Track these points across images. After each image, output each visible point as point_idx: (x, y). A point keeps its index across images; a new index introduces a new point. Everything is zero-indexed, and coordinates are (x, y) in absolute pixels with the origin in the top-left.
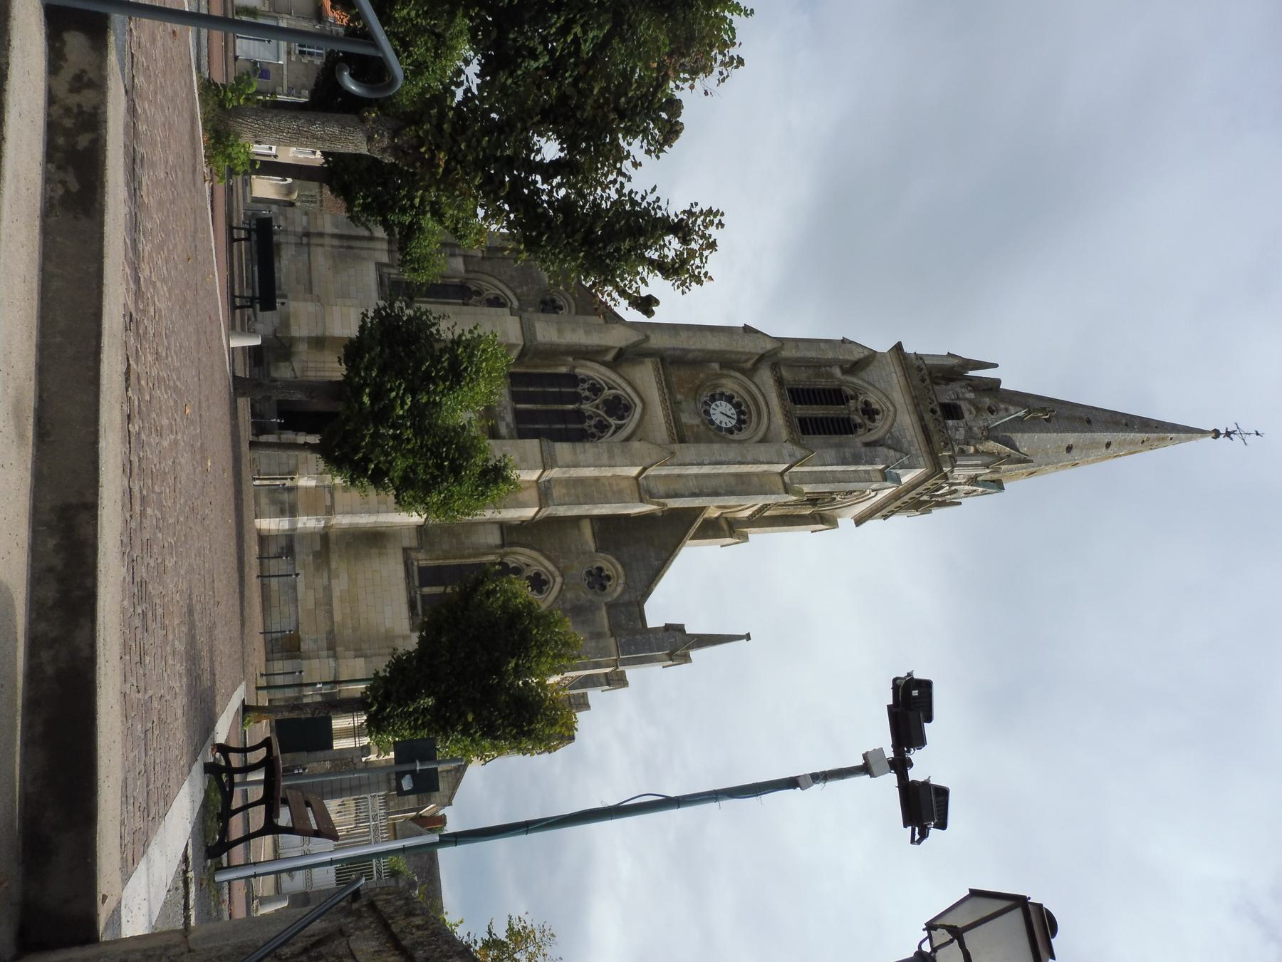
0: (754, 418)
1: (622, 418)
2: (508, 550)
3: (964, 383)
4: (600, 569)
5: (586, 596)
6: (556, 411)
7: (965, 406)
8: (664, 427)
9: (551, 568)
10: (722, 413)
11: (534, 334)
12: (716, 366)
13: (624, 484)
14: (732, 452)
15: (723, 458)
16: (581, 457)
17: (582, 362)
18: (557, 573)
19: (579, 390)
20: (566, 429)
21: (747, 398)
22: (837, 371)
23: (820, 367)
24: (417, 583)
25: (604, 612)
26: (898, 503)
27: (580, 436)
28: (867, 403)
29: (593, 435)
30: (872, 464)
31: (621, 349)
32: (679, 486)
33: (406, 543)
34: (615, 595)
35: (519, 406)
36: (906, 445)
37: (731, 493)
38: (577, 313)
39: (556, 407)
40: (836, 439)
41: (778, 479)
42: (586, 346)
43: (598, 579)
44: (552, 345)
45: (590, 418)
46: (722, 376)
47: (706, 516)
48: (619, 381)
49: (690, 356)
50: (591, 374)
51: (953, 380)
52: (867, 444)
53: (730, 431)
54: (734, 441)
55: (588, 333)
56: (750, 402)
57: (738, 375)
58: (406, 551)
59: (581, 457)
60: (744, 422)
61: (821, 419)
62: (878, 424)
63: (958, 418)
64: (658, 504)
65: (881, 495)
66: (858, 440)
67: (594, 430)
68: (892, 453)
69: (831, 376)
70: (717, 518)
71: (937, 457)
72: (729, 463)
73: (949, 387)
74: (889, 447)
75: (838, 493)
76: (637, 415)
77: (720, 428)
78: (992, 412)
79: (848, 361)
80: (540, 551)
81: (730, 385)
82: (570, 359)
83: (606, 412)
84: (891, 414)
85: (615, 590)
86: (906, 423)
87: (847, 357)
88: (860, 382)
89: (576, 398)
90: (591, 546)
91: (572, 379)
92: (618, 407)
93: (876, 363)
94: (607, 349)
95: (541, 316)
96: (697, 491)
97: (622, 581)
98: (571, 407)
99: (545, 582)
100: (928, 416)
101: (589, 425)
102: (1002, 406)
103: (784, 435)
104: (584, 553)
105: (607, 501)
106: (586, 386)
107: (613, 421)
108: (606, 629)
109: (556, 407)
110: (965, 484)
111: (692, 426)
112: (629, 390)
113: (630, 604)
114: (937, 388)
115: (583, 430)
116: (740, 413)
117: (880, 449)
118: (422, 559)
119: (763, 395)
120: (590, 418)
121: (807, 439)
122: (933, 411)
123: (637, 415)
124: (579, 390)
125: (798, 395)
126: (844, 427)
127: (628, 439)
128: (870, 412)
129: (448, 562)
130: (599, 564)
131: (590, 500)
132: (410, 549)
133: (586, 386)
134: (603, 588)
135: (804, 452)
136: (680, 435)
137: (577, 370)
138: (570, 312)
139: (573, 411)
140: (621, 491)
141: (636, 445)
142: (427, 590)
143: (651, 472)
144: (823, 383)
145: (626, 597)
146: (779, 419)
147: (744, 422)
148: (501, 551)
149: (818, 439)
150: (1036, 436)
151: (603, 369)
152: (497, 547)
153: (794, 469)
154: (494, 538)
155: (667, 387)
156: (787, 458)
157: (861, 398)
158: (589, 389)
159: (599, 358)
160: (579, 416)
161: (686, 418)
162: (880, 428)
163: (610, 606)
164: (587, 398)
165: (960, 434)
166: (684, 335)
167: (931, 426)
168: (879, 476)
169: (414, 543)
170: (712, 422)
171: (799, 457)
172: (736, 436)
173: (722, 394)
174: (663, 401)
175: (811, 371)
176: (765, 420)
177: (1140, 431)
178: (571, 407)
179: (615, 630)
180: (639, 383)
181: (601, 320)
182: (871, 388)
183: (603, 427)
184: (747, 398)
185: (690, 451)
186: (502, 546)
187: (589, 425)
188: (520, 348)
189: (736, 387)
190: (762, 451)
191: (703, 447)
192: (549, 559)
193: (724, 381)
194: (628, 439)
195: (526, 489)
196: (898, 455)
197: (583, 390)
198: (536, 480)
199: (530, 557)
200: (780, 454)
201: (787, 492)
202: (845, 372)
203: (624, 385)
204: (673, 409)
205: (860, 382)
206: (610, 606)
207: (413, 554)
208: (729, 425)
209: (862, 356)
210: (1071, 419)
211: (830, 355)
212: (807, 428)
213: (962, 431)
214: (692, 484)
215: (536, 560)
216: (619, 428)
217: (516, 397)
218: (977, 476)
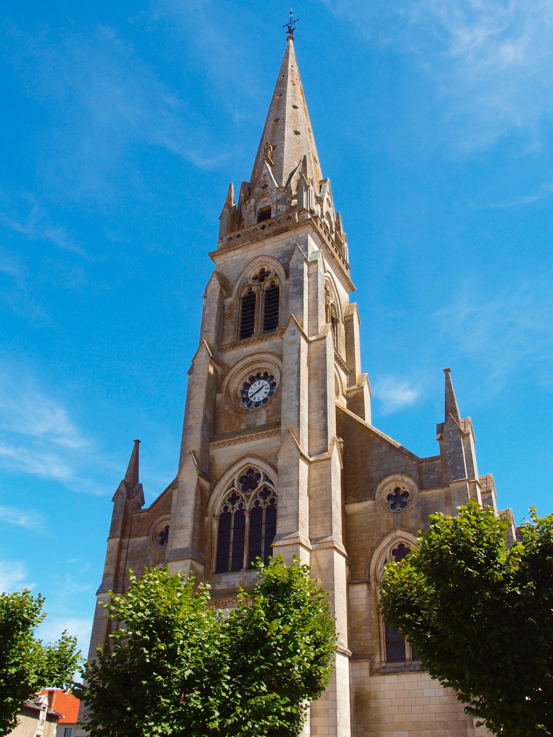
0: (263, 365)
1: (259, 476)
2: (372, 578)
3: (243, 207)
4: (390, 497)
5: (412, 510)
6: (250, 532)
7: (260, 206)
8: (267, 439)
9: (388, 540)
10: (259, 391)
11: (183, 550)
12: (219, 396)
13: (314, 473)
14: (289, 382)
15: (295, 389)
16: (290, 510)
17: (209, 509)
18: (393, 535)
19: (264, 507)
20: (234, 529)
21: (245, 371)
22: (229, 301)
23: (224, 314)
24: (402, 664)
25: (424, 493)
26: (336, 256)
27: (272, 511)
28: (255, 278)
29: (273, 500)
30: (302, 271)
31: (199, 475)
32: (317, 427)
33: (366, 673)
34: (412, 483)
35: (244, 566)
36: (289, 247)
37: (324, 383)
38: (170, 513)
39: (247, 533)
40: (282, 300)
41: (313, 345)
42: (196, 505)
43: (398, 499)
44: (193, 535)
45: (257, 502)
46: (228, 391)
47: (345, 407)
48: (227, 477)
49: (209, 417)
50: (220, 502)
51: (241, 216)
52: (287, 276)
53: (273, 385)
54: (281, 381)
55: (184, 503)
56: (250, 368)
57: (227, 379)
58: (373, 672)
59: (290, 510)
60: (266, 374)
61: (266, 312)
62: (271, 268)
63: (270, 210)
64: (332, 445)
65: (328, 267)
66: (283, 283)
67: (268, 500)
68: (294, 256)
69: (231, 305)
70: (347, 399)
71: (299, 223)
72: (299, 384)
73: (245, 218)
74: (290, 259)
75: (327, 301)
76: (256, 462)
77: (270, 394)
78: (266, 186)
79: (221, 292)
80: (373, 549)
81: (236, 385)
82: (207, 519)
83: (253, 489)
84: (264, 259)
85: (407, 483)
86: (272, 246)
87: (217, 293)
88: (238, 283)
89: (240, 515)
90: (368, 504)
91: (224, 518)
92: (249, 479)
93: (224, 272)
94: (200, 487)
95: (170, 542)
96: (322, 412)
97: (399, 477)
98: (247, 519)
99: (401, 546)
100: (267, 231)
101: (263, 504)
102: (262, 179)
103: (276, 340)
104: (375, 510)
105: (328, 490)
106: (230, 506)
107: (261, 483)
108: (442, 491)
109: (247, 533)
110: (322, 206)
111: (268, 416)
112: (235, 469)
113: (419, 471)
114: (245, 226)
115: (268, 509)
116: (258, 377)
117: (291, 266)
118: (380, 658)
119: (244, 358)
120: (257, 502)
121: (281, 322)
122: (263, 228)
123: (257, 462)
124: (264, 507)
125: (246, 332)
126: (273, 294)
127: (276, 470)
128: (262, 275)
129: (383, 634)
130: (385, 497)
131: (328, 503)
132: (371, 669)
133: (230, 506)
134: (406, 494)
135: (291, 324)
136: (274, 425)
137: (217, 513)
138: (169, 519)
139: (251, 517)
140: (321, 476)
141: (280, 463)
142: (408, 655)
143: (305, 451)
144: (237, 312)
145: (415, 473)
146: (265, 345)
147: (266, 374)
148: (373, 585)
149: (282, 314)
150: (286, 154)
151: (217, 491)
152: (369, 589)
153: (306, 331)
154: (361, 590)
155: (237, 435)
156: (295, 337)
157: (250, 282)
158: (233, 504)
159: (207, 494)
160: (256, 512)
161: (262, 420)
162: (275, 267)
163: (422, 487)
164: (241, 505)
165: (282, 208)
166: (191, 422)
167: (275, 228)
168: (313, 266)
169: (366, 665)
170: (265, 400)
171: (295, 327)
172: (277, 380)
173: (243, 392)
174: (246, 440)
175: (227, 321)
176: (266, 356)
177: (286, 86)
178: (247, 519)
179: (440, 483)
180: (229, 461)
181: (175, 492)
182: (243, 275)
183: (266, 492)
184: (245, 371)
185: (287, 416)
186: (368, 583)
187: (263, 504)
188: (194, 563)
189: (237, 380)
190: (289, 358)
191: (284, 406)
192: (380, 541)
193: (232, 390)
194: (276, 470)
195: (317, 561)
196: (296, 252)
197: (234, 509)
198: (313, 547)
199: (379, 559)
200: (292, 343)
201: (325, 338)
202: (229, 295)
203: (230, 473)
204: (254, 430)
205: (238, 283)
206: (422, 487)
207: (377, 666)
208: (268, 386)
209: (217, 282)
210: (274, 132)
211: (215, 306)
212: (272, 324)
213: (280, 207)
214: (316, 416)
215: (381, 554)
216: (267, 478)
217: (237, 568)
218: (316, 197)
